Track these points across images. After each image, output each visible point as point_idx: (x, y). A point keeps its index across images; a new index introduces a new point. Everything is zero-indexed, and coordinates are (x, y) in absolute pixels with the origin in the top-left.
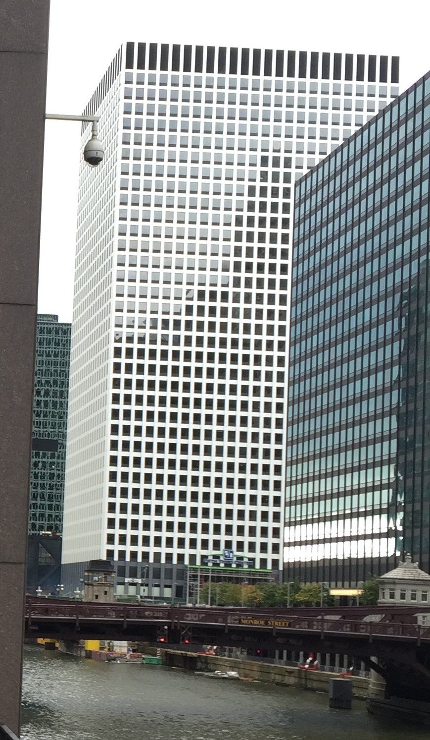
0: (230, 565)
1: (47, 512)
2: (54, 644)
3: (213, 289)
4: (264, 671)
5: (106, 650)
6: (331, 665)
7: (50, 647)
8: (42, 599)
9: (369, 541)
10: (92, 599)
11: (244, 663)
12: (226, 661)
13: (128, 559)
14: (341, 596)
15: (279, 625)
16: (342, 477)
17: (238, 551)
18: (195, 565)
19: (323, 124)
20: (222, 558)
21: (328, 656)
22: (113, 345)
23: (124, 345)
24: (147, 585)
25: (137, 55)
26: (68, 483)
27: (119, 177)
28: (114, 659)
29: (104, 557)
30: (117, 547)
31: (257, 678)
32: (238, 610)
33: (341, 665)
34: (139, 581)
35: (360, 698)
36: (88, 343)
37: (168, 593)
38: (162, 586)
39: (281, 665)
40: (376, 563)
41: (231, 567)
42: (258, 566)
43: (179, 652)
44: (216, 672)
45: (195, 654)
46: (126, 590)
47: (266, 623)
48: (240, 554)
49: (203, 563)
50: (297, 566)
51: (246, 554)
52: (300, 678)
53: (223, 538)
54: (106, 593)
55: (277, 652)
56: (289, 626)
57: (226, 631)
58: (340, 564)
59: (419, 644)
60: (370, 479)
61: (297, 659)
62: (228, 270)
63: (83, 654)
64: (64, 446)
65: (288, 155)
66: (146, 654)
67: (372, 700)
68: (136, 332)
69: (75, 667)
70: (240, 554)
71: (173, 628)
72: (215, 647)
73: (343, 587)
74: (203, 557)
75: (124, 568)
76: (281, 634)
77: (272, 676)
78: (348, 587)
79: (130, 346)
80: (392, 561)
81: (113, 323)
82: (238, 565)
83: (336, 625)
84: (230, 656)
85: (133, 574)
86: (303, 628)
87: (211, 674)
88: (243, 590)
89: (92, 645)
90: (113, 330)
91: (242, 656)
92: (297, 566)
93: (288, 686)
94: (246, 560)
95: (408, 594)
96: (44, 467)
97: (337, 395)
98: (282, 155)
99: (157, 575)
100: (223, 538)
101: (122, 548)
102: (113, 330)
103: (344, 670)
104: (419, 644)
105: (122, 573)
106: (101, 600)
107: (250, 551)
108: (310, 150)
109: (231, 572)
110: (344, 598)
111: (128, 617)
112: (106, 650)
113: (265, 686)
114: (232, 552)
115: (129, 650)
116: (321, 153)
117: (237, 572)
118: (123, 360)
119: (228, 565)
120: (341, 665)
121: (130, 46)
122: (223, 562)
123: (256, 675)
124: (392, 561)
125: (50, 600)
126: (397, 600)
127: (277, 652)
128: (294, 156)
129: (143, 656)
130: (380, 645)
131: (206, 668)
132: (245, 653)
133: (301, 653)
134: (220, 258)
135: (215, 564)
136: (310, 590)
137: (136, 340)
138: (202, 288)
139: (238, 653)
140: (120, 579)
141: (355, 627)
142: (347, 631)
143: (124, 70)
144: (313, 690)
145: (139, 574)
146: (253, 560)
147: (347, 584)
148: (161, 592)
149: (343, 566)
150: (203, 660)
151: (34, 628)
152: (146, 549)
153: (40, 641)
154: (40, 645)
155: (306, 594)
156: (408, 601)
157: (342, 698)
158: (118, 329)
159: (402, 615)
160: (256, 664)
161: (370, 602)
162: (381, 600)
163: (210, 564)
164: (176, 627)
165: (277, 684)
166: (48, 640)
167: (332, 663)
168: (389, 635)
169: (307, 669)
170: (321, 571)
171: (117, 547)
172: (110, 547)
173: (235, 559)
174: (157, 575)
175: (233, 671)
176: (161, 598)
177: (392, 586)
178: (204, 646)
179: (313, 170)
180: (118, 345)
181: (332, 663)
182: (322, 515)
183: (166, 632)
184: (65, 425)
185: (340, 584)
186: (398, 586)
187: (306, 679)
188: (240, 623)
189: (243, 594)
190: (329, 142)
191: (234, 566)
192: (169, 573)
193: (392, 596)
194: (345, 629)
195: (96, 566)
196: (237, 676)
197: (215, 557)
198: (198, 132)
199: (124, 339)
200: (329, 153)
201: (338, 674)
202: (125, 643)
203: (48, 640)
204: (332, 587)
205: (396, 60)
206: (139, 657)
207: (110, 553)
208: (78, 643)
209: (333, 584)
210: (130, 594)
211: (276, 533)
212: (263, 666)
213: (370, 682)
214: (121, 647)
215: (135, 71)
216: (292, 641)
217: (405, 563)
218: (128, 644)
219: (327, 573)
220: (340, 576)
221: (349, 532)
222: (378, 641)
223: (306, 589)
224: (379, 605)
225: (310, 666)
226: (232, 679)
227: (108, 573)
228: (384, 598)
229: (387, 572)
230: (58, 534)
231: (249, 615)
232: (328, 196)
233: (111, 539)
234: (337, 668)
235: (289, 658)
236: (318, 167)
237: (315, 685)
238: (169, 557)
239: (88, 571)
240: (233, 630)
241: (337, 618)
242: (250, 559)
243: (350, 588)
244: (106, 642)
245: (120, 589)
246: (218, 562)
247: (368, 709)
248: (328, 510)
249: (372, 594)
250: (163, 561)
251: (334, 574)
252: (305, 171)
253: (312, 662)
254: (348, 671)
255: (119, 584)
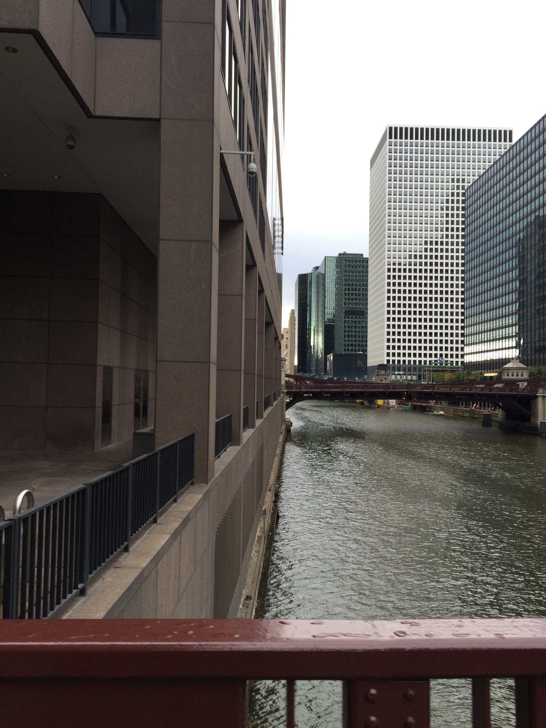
1: (361, 343)
3: (431, 240)
7: (362, 403)
8: (357, 383)
9: (507, 350)
15: (456, 390)
16: (491, 322)
19: (477, 162)
22: (387, 267)
23: (392, 267)
24: (405, 375)
25: (394, 133)
26: (369, 330)
27: (388, 189)
28: (390, 408)
29: (385, 363)
30: (391, 358)
33: (488, 407)
34: (402, 373)
35: (496, 421)
36: (375, 267)
37: (414, 378)
40: (495, 361)
42: (454, 364)
45: (425, 405)
46: (396, 378)
47: (450, 389)
48: (446, 359)
49: (430, 364)
50: (486, 362)
51: (449, 359)
52: (470, 413)
53: (439, 352)
60: (501, 324)
61: (469, 405)
62: (438, 231)
63: (376, 406)
64: (367, 313)
65: (463, 177)
67: (500, 422)
68: (397, 261)
70: (446, 359)
73: (490, 372)
74: (430, 361)
75: (395, 367)
76: (457, 394)
79: (394, 267)
80: (507, 360)
81: (386, 257)
82: (446, 365)
83: (482, 389)
85: (399, 370)
87: (432, 413)
88: (447, 375)
89: (380, 402)
90: (387, 260)
92: (486, 362)
93: (465, 417)
94: (449, 362)
95: (515, 374)
96: (359, 323)
97: (486, 286)
98: (461, 177)
99: (409, 370)
100: (439, 352)
101: (394, 358)
102: (387, 260)
103: (490, 409)
106: (384, 382)
108: (471, 174)
109: (443, 367)
110: (491, 377)
113: (456, 417)
116: (504, 149)
117: (445, 367)
118: (392, 274)
119: (441, 364)
121: (391, 128)
123: (452, 413)
124: (507, 360)
126: (510, 377)
128: (466, 177)
134: (434, 226)
136: (475, 374)
137: (397, 264)
138: (426, 240)
140: (393, 372)
143: (388, 140)
144: (476, 418)
146: (453, 362)
147: (489, 371)
148: (412, 377)
149: (496, 363)
151: (347, 395)
153: (357, 401)
154: (358, 403)
156: (515, 377)
157: (487, 421)
158: (389, 260)
159: (513, 384)
160: (452, 408)
161: (499, 379)
165: (461, 416)
167: (485, 406)
171: (391, 358)
172: (388, 358)
174: (409, 370)
176: (412, 380)
179: (502, 157)
180: (389, 267)
181: (485, 406)
182: (489, 339)
184: (367, 304)
187: (473, 413)
188: (438, 389)
190: (487, 164)
193: (508, 375)
195: (381, 367)
197: (435, 361)
198: (407, 195)
199: (392, 264)
200: (508, 148)
201: (486, 411)
202: (394, 401)
203: (361, 401)
205: (511, 132)
207: (388, 361)
208: (374, 401)
209: (486, 371)
211: (462, 349)
212: (454, 409)
213: (499, 413)
215: (393, 140)
216: (462, 397)
221: (498, 348)
222: (501, 396)
226: (441, 415)
227: (386, 370)
232: (476, 200)
233: (388, 355)
234: (486, 408)
235: (466, 405)
236: (483, 175)
237: (477, 416)
239: (377, 369)
245: (393, 377)
248: (483, 338)
249: (500, 374)
251: (486, 367)
252: (477, 178)
253: (476, 406)
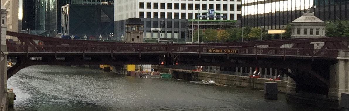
0: (213, 18)
2: (110, 68)
4: (230, 80)
5: (139, 70)
6: (267, 75)
7: (107, 70)
8: (101, 42)
10: (130, 41)
11: (218, 76)
12: (208, 74)
13: (159, 17)
14: (275, 34)
17: (217, 10)
18: (234, 20)
20: (208, 14)
21: (266, 69)
24: (164, 32)
28: (144, 75)
29: (138, 16)
31: (226, 83)
32: (207, 44)
33: (273, 74)
34: (159, 29)
35: (283, 93)
37: (176, 36)
38: (173, 32)
39: (239, 75)
41: (213, 19)
42: (229, 18)
43: (181, 70)
44: (203, 81)
45: (190, 71)
46: (152, 36)
47: (223, 51)
48: (218, 12)
49: (196, 18)
52: (250, 82)
54: (138, 37)
55: (237, 68)
56: (237, 52)
57: (200, 57)
58: (281, 14)
59: (313, 60)
61: (248, 72)
63: (126, 73)
66: (162, 72)
67: (288, 94)
69: (121, 80)
70: (218, 12)
71: (168, 56)
72: (202, 67)
73: (276, 29)
77: (235, 82)
78: (278, 28)
80: (298, 13)
82: (217, 18)
84: (210, 71)
85: (156, 26)
86: (246, 53)
87: (199, 83)
89: (131, 68)
91: (217, 71)
93: (243, 87)
94: (222, 15)
95: (308, 31)
99: (170, 26)
103: (275, 77)
104: (313, 60)
105: (149, 25)
106: (136, 41)
107: (224, 10)
109: (213, 22)
111: (142, 51)
112: (139, 70)
113: (231, 88)
114: (213, 11)
115: (152, 70)
117: (217, 22)
119: (211, 18)
120: (273, 74)
122: (208, 17)
123: (225, 82)
124: (298, 13)
125: (105, 43)
126: (302, 35)
127: (237, 68)
129: (161, 73)
130: (291, 61)
131: (197, 79)
132: (219, 70)
133: (251, 68)
135: (203, 18)
136: (256, 31)
139: (215, 70)
140: (148, 29)
141: (276, 52)
142: (271, 54)
145: (159, 25)
146: (226, 15)
148: (173, 36)
149: (283, 16)
150: (195, 74)
152: (232, 12)
153: (101, 66)
154: (102, 69)
155: (254, 34)
156: (308, 35)
157: (272, 93)
159: (304, 44)
160: (226, 75)
161: (287, 38)
162: (293, 35)
163: (201, 18)
164: (170, 55)
165: (238, 87)
166: (106, 66)
167: (268, 73)
168: (298, 55)
169: (253, 77)
170: (266, 19)
171: (146, 10)
172: (142, 10)
173: (215, 15)
174: (170, 26)
175: (212, 80)
176: (172, 39)
177: (298, 27)
178: (196, 66)
181: (268, 73)
183: (165, 59)
185: (274, 27)
186: (303, 27)
187: (253, 83)
188: (208, 51)
189: (218, 35)
191: (215, 19)
192: (177, 24)
193: (299, 33)
194: (204, 51)
195: (132, 21)
196: (214, 83)
197: (203, 14)
201: (270, 80)
203: (106, 66)
204: (269, 29)
206: (158, 74)
207: (142, 14)
208: (123, 67)
209: (270, 27)
210: (154, 37)
212: (228, 77)
213: (288, 83)
214: (148, 68)
216: (239, 61)
217: (306, 13)
218: (152, 66)
219: (263, 21)
220: (278, 22)
222: (289, 59)
223: (254, 30)
224: (292, 38)
225: (255, 76)
226: (212, 85)
227: (139, 26)
228: (294, 34)
229: (296, 19)
230: (112, 4)
231: (213, 47)
234: (265, 75)
235: (244, 71)
237: (259, 86)
238: (177, 15)
239: (128, 25)
240: (204, 56)
241: (266, 46)
242: (224, 14)
243: (280, 29)
244: (139, 66)
245: (148, 35)
246: (206, 17)
247: (286, 99)
250: (173, 17)
251: (270, 22)
253: (257, 73)
254: (277, 78)
255: (147, 31)
